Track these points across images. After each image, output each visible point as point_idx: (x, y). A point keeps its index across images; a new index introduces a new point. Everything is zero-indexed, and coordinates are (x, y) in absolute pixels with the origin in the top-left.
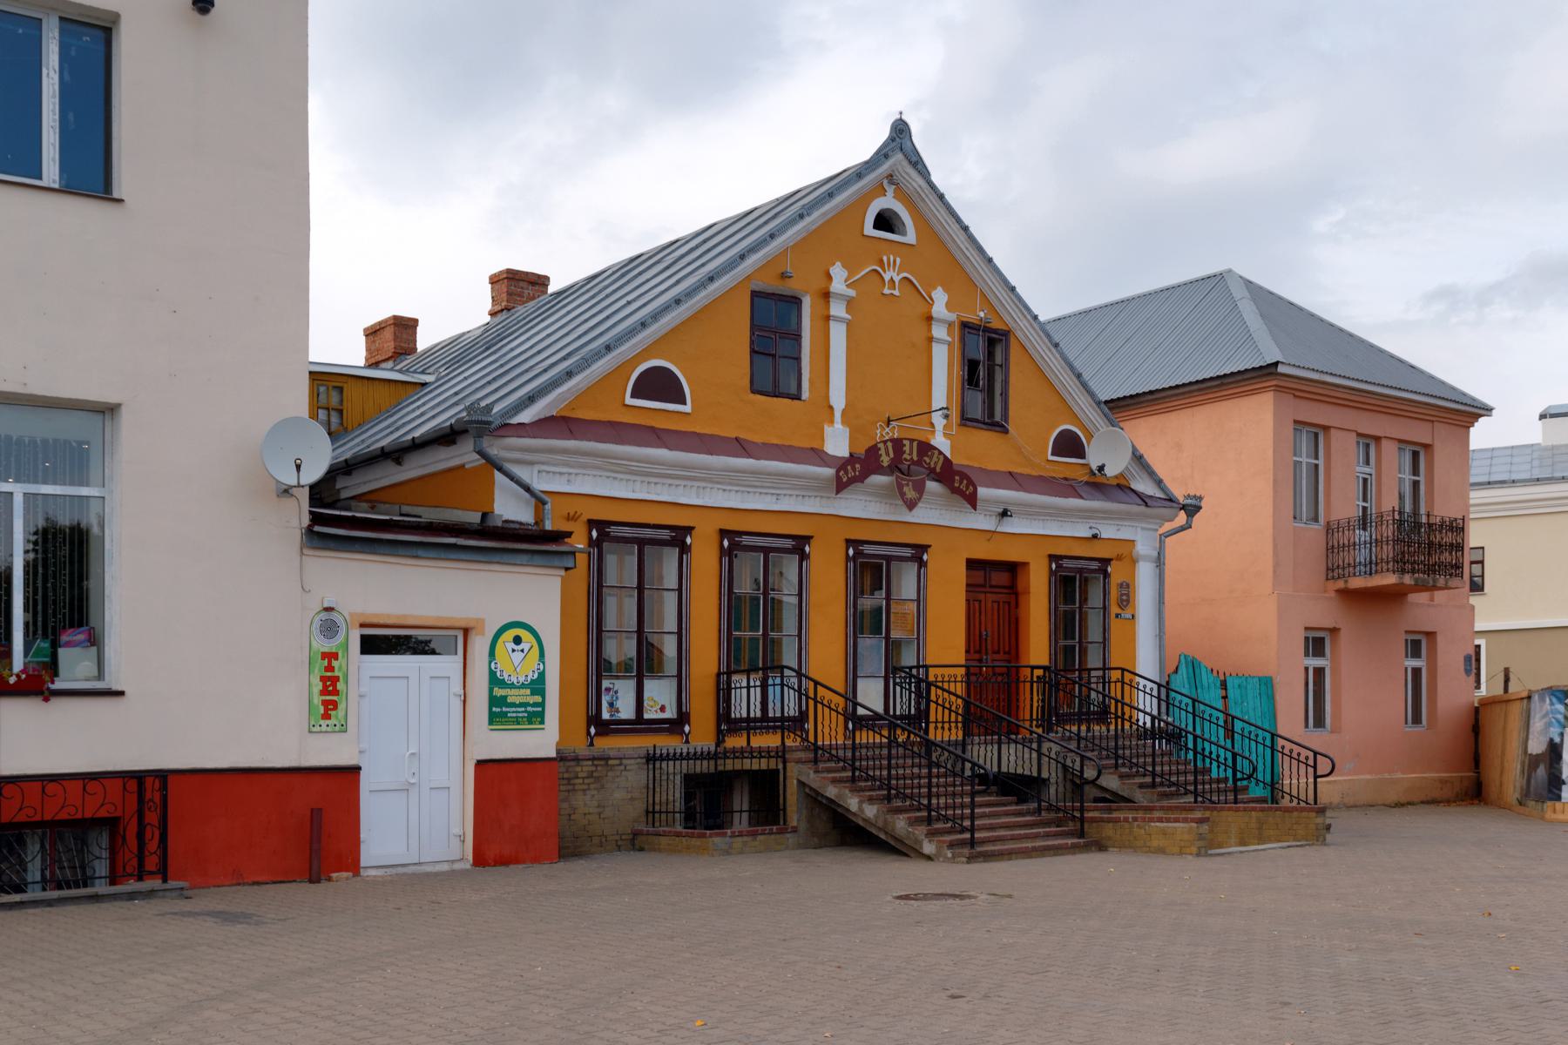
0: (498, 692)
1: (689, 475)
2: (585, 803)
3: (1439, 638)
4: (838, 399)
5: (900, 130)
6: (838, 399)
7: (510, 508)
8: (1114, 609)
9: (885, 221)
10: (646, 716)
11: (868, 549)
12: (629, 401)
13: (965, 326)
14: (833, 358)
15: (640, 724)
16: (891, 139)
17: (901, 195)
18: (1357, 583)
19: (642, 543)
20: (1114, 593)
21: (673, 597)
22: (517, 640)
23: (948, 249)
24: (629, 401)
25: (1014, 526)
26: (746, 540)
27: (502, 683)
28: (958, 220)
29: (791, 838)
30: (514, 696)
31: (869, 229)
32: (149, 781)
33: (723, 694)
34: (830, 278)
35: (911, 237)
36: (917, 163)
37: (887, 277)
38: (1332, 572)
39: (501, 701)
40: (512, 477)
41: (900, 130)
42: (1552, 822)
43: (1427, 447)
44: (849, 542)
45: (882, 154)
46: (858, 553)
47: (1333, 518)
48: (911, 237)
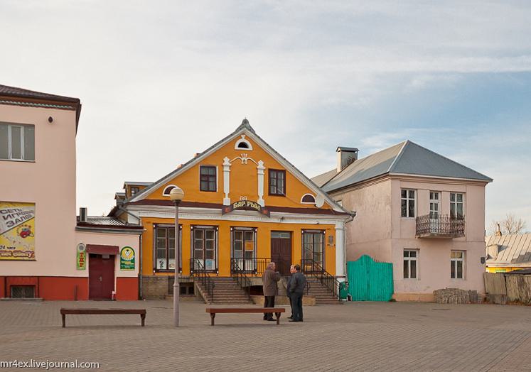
0: (123, 262)
1: (206, 213)
2: (151, 288)
3: (467, 252)
4: (227, 191)
5: (245, 122)
6: (227, 191)
7: (131, 221)
8: (327, 243)
9: (243, 145)
10: (170, 268)
11: (198, 227)
12: (164, 195)
13: (270, 170)
14: (225, 181)
15: (204, 271)
16: (242, 124)
17: (247, 138)
18: (422, 236)
19: (313, 233)
20: (327, 238)
21: (321, 245)
22: (128, 251)
23: (263, 151)
24: (164, 195)
25: (284, 222)
26: (307, 231)
27: (124, 260)
28: (265, 143)
29: (194, 298)
30: (126, 263)
31: (236, 147)
32: (8, 279)
33: (192, 263)
34: (224, 161)
35: (250, 148)
36: (251, 130)
37: (242, 159)
38: (418, 233)
39: (124, 264)
40: (131, 214)
41: (245, 122)
42: (151, 327)
43: (464, 193)
44: (302, 230)
45: (240, 128)
46: (234, 230)
47: (419, 216)
48: (250, 148)
